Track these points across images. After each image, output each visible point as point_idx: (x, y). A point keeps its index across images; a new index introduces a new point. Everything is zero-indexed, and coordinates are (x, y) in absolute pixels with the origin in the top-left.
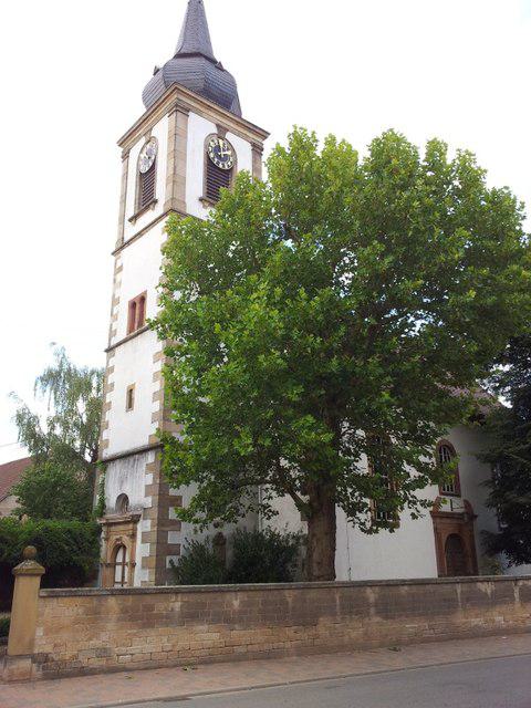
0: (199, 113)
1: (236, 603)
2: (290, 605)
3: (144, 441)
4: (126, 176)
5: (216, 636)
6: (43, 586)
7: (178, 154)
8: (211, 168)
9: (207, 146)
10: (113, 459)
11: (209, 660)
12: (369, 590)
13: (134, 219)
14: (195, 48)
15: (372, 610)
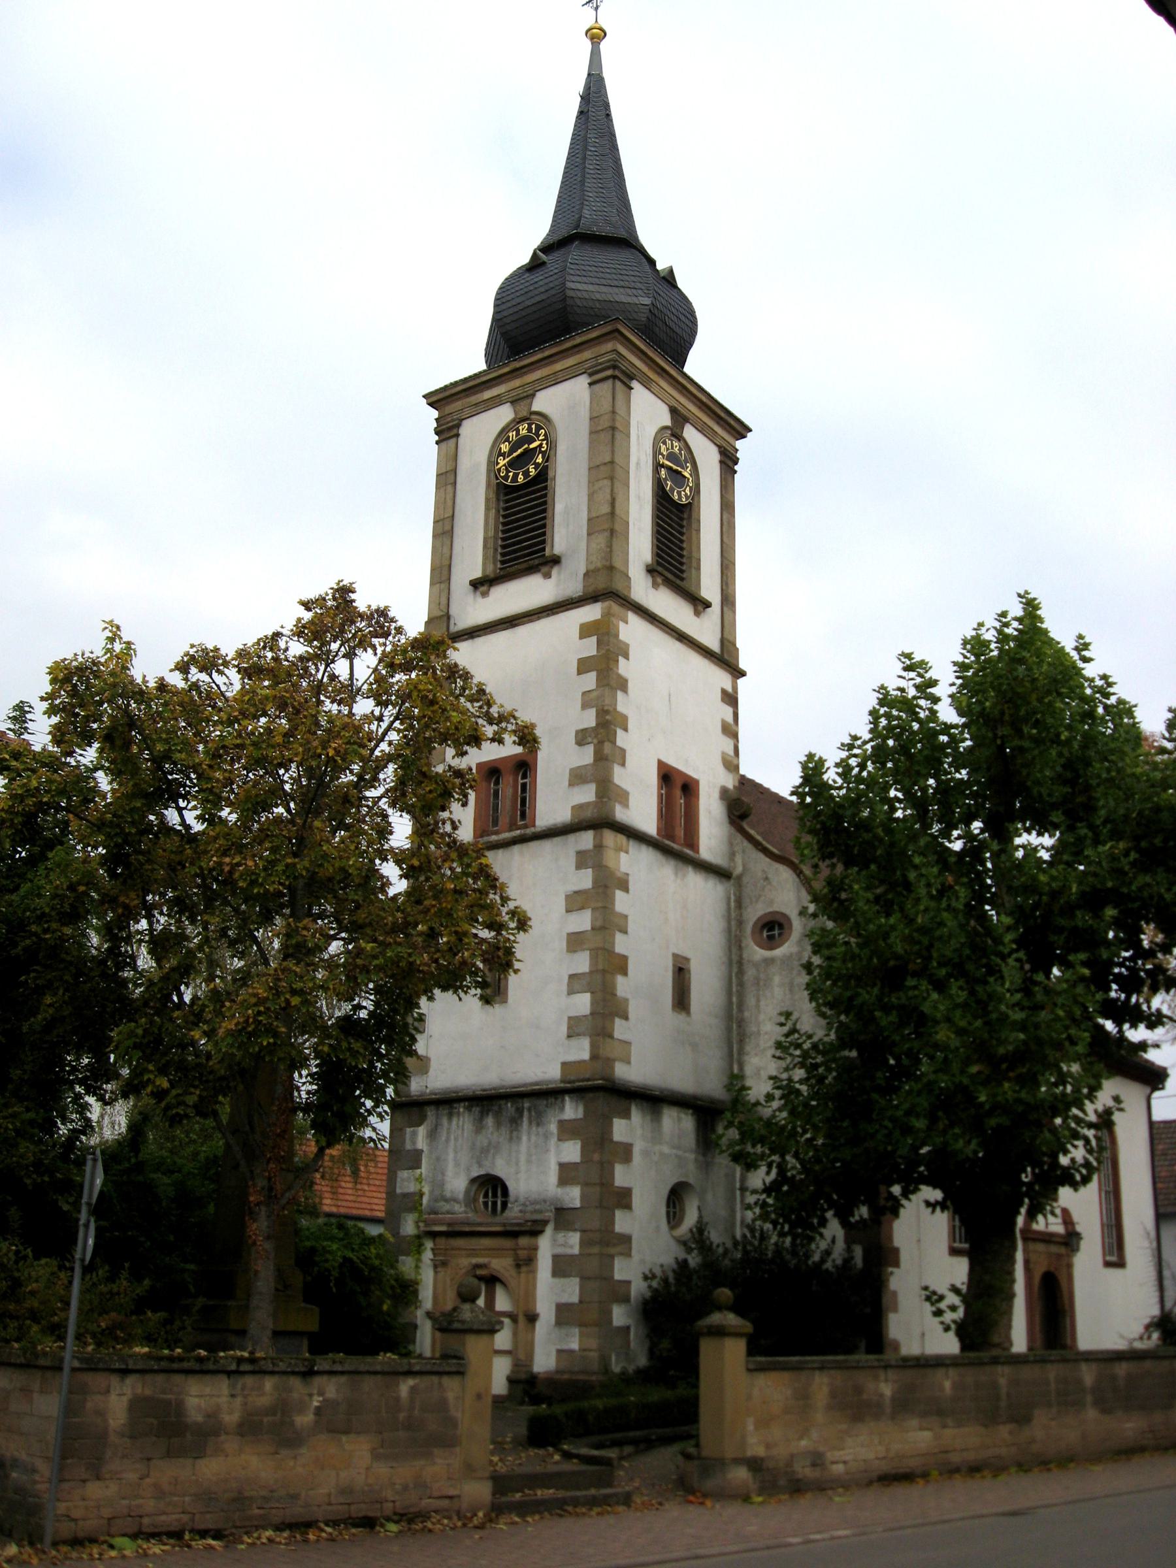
0: (647, 384)
1: (947, 1384)
2: (1004, 1391)
3: (549, 1071)
4: (447, 478)
5: (927, 1435)
6: (751, 1352)
7: (608, 471)
8: (662, 498)
9: (656, 452)
10: (447, 1102)
11: (1128, 1452)
12: (1084, 1367)
13: (481, 585)
14: (593, 213)
15: (1089, 1399)
